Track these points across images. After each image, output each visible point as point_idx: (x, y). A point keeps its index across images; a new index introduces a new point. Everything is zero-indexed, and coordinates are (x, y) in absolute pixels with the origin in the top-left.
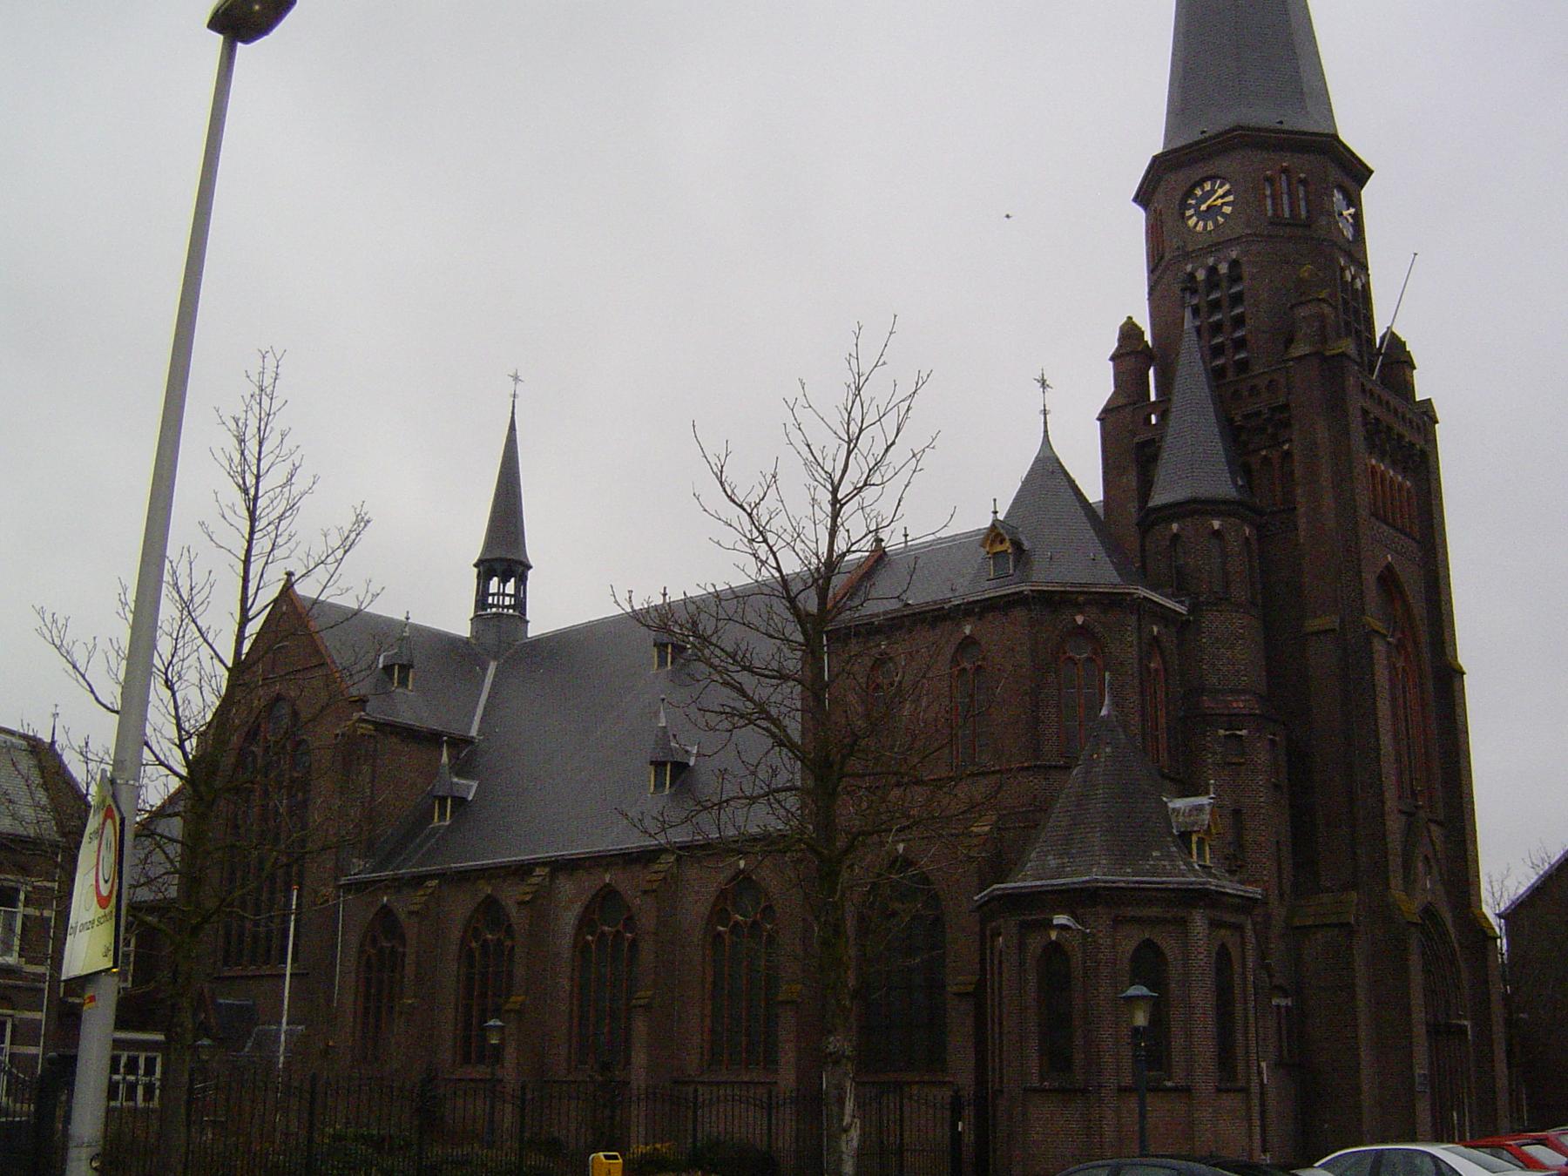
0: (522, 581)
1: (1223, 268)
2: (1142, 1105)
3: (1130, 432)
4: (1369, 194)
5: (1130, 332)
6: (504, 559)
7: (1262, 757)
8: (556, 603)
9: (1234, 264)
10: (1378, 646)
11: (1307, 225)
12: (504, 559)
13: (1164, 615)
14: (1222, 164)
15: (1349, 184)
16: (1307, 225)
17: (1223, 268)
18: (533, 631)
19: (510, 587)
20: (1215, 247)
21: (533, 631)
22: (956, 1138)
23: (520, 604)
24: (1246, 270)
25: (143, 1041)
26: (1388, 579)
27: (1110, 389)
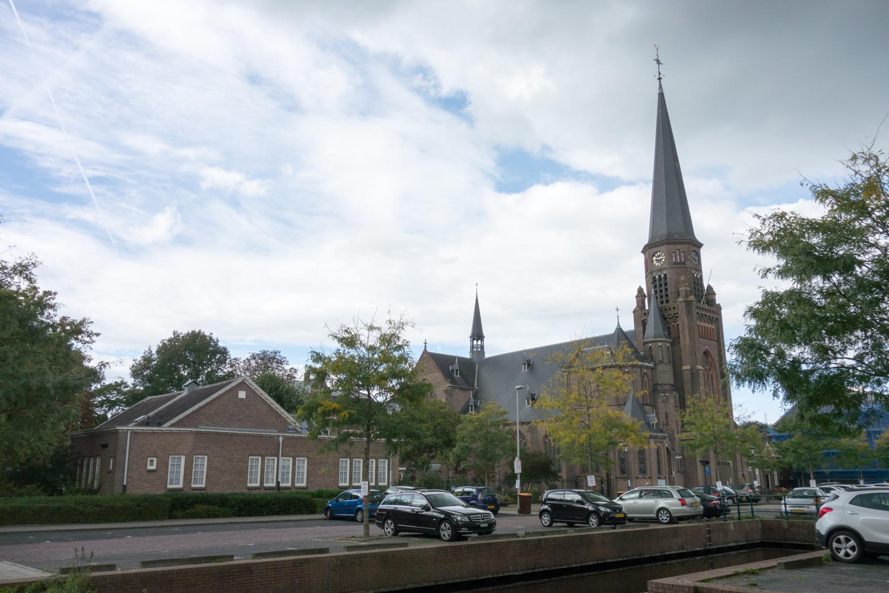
0: (482, 340)
1: (662, 276)
2: (263, 460)
3: (640, 315)
4: (703, 251)
5: (640, 290)
6: (477, 334)
7: (672, 401)
8: (494, 347)
9: (665, 275)
10: (700, 372)
11: (684, 263)
12: (477, 334)
13: (648, 368)
14: (664, 248)
15: (696, 249)
16: (684, 263)
17: (662, 276)
18: (487, 355)
19: (479, 342)
20: (660, 270)
21: (487, 355)
22: (602, 488)
23: (482, 347)
24: (668, 276)
25: (185, 468)
26: (706, 353)
27: (635, 305)
